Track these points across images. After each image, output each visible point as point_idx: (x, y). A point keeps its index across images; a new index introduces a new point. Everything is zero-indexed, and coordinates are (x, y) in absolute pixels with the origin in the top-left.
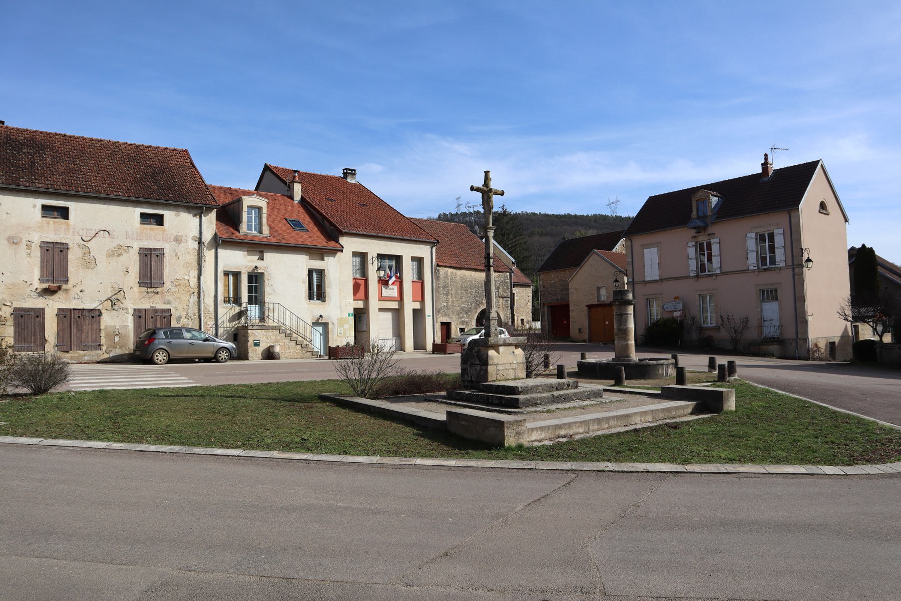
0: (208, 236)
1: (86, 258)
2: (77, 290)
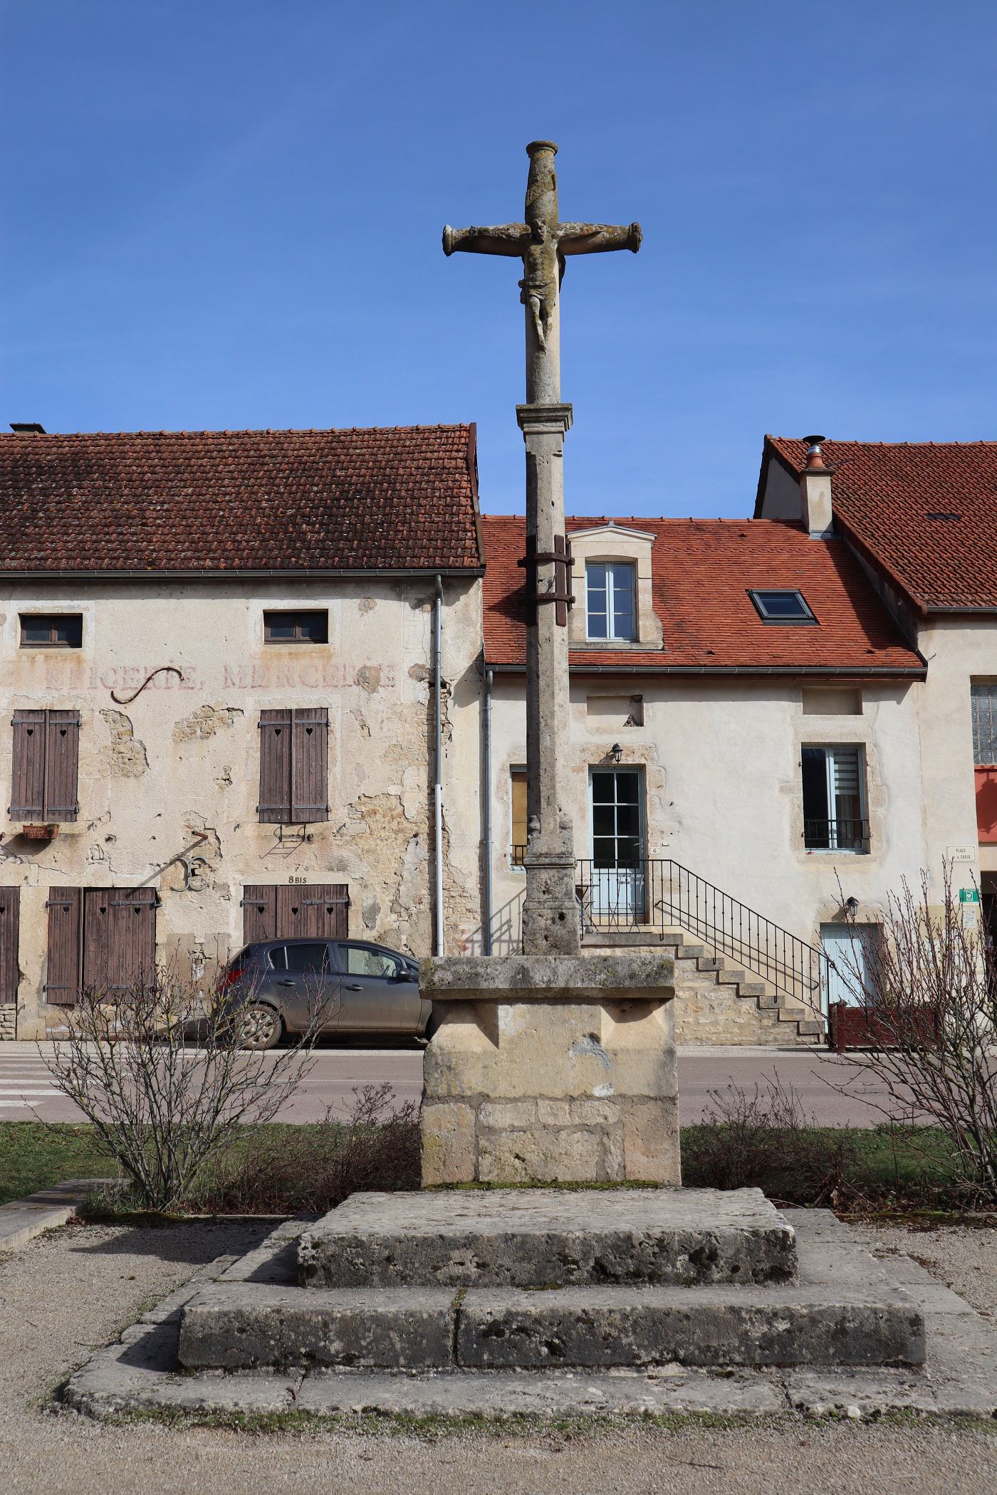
0: (456, 664)
1: (122, 749)
2: (98, 835)
